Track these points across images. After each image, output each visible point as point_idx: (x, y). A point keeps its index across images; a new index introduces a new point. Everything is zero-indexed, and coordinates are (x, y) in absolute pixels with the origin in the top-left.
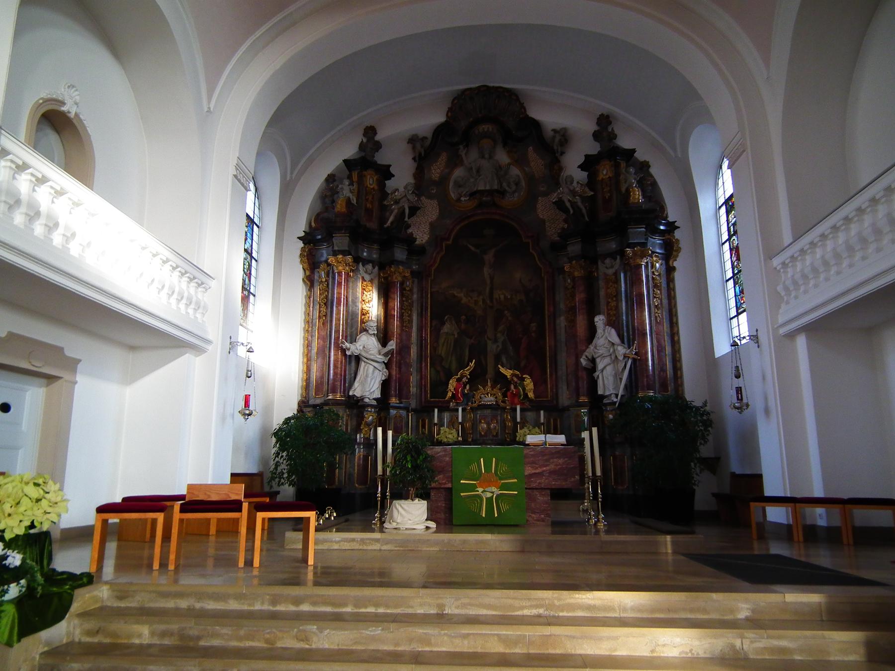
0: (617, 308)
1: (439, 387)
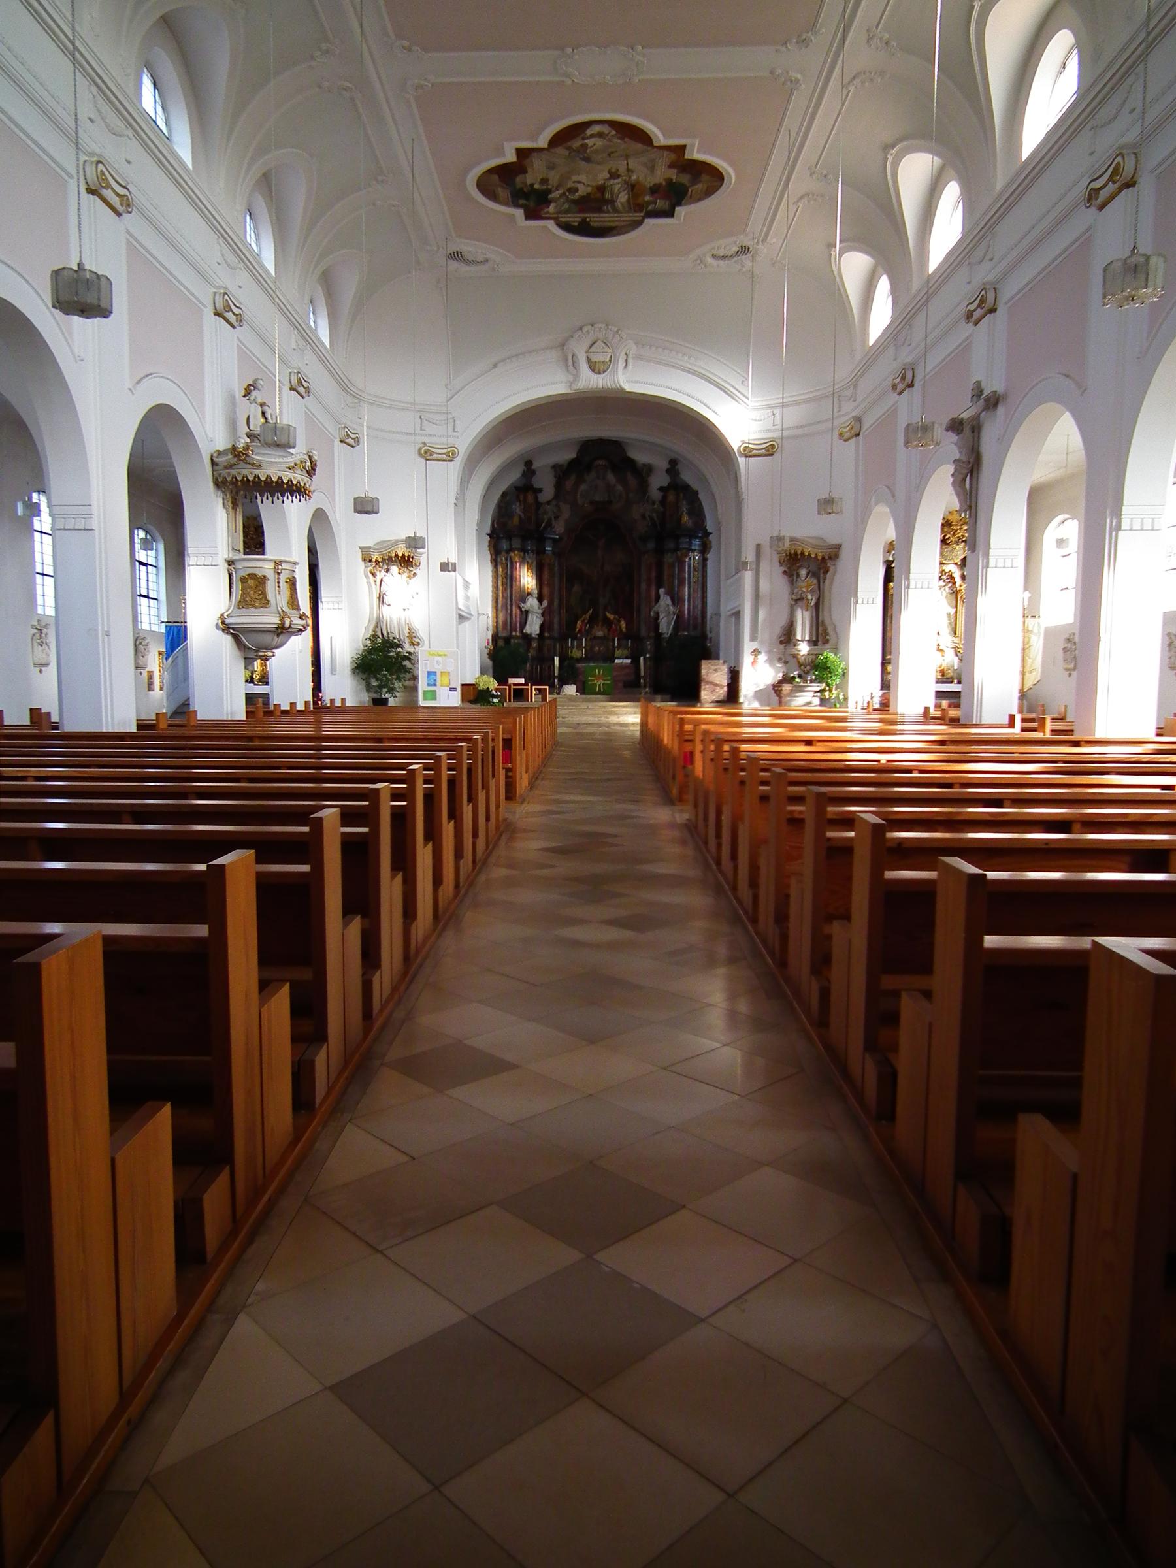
0: (673, 583)
1: (571, 624)
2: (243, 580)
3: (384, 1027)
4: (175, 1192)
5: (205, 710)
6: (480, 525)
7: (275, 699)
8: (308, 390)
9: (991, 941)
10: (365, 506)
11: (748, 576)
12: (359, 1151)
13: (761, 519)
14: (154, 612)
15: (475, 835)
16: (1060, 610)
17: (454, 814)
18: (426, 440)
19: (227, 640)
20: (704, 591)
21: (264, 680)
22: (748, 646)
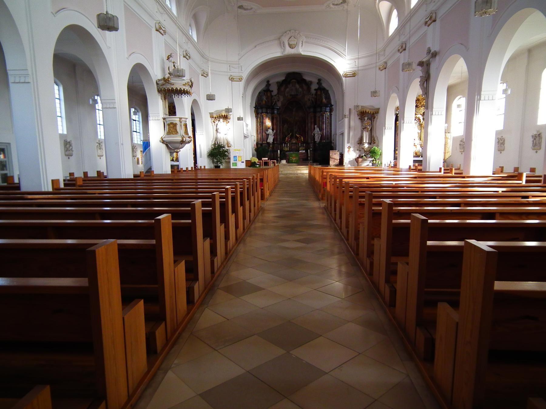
1: (284, 139)
2: (169, 125)
3: (219, 276)
4: (146, 330)
5: (157, 171)
6: (251, 104)
7: (181, 167)
8: (189, 57)
9: (429, 243)
10: (210, 98)
11: (346, 120)
12: (209, 317)
13: (351, 99)
14: (139, 137)
15: (250, 211)
16: (458, 130)
17: (242, 204)
18: (232, 74)
19: (164, 146)
20: (331, 126)
21: (177, 160)
22: (346, 145)
